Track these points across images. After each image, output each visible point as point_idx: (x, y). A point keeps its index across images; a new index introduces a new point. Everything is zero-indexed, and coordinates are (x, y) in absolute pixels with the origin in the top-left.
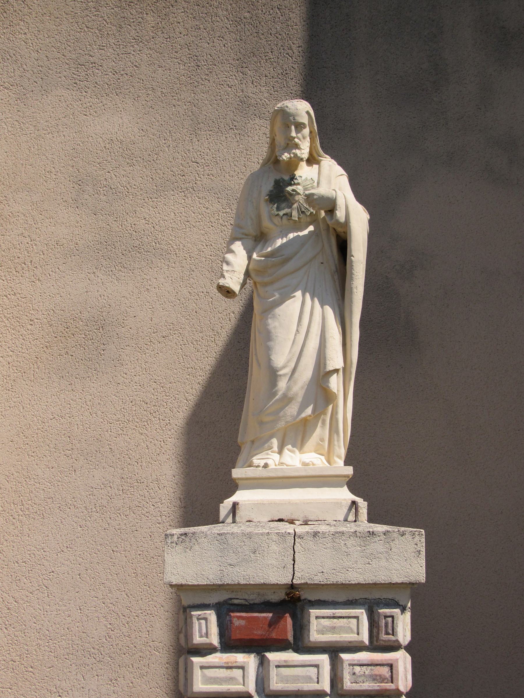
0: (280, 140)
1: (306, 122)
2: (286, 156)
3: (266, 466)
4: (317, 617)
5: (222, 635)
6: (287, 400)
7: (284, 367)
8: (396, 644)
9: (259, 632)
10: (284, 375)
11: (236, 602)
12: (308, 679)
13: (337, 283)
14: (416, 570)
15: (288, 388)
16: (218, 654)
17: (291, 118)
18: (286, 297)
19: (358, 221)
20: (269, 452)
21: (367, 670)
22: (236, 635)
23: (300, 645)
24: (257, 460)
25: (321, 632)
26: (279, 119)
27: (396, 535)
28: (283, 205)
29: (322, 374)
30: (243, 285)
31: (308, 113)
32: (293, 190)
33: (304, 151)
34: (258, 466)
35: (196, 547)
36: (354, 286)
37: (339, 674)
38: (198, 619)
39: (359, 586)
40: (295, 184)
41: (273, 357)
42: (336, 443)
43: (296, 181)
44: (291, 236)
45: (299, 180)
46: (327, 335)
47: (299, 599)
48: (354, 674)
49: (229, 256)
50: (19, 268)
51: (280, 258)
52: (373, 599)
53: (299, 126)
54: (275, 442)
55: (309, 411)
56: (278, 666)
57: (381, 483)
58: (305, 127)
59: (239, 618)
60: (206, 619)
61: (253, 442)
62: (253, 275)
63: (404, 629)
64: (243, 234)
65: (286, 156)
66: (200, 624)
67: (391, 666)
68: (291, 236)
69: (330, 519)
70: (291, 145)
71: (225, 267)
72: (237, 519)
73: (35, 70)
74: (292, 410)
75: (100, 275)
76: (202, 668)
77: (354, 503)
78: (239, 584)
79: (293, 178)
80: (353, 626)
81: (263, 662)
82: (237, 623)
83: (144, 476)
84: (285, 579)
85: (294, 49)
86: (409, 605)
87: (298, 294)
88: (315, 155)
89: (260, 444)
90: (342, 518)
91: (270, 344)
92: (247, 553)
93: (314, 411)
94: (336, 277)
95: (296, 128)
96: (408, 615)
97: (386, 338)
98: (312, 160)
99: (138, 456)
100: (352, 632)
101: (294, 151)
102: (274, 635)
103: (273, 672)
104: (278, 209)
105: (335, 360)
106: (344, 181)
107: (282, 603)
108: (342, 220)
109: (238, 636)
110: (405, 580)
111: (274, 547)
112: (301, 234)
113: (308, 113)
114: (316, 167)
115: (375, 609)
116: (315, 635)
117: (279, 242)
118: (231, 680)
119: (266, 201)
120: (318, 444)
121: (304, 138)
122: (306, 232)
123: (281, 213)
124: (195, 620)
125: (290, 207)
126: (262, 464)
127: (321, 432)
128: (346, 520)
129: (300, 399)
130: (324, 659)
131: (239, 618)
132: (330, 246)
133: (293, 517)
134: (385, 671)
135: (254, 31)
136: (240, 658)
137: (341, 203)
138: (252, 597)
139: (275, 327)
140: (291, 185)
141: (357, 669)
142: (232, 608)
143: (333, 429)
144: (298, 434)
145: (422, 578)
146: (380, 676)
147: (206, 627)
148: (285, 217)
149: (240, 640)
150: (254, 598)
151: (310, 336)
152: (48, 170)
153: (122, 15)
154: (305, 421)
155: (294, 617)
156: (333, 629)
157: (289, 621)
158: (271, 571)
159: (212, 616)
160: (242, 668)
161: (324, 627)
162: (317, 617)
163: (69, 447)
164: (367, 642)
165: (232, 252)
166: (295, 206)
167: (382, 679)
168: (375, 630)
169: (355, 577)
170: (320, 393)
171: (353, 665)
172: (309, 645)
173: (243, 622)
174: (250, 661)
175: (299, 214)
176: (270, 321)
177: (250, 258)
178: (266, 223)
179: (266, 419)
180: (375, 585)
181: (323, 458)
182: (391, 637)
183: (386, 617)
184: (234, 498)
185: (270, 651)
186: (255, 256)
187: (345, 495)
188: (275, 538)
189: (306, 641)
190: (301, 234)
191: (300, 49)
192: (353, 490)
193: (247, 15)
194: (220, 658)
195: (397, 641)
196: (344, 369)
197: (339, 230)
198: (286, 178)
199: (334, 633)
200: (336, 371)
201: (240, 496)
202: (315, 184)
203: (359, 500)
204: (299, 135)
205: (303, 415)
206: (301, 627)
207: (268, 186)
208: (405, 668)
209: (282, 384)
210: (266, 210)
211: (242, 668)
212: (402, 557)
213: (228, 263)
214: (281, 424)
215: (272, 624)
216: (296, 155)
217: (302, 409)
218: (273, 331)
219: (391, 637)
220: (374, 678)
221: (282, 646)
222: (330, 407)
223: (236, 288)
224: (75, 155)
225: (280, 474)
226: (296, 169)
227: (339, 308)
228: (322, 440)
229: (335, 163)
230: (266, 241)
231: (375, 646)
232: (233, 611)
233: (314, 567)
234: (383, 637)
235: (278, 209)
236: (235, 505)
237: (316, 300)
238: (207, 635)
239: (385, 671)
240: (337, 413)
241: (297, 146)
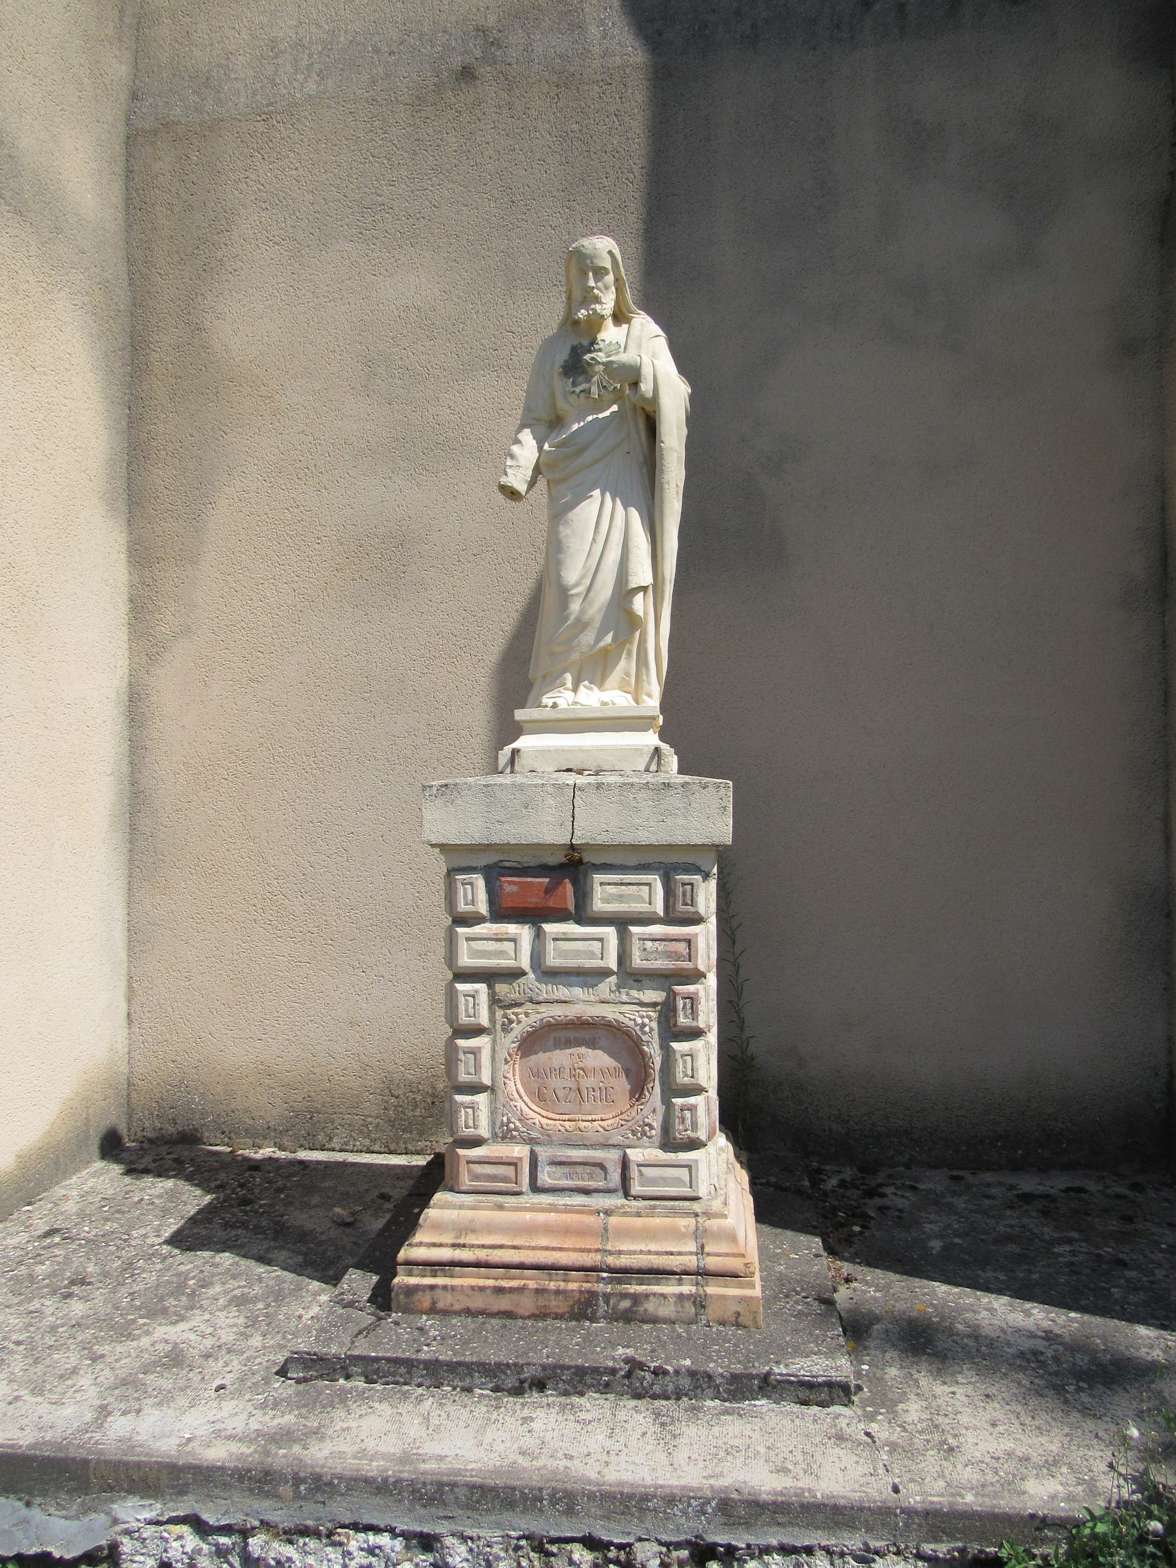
0: (577, 294)
1: (609, 266)
2: (582, 314)
3: (555, 706)
4: (602, 884)
5: (491, 902)
6: (581, 625)
7: (577, 585)
8: (696, 916)
9: (534, 900)
10: (578, 595)
11: (507, 864)
12: (592, 955)
13: (646, 479)
14: (722, 830)
15: (582, 611)
16: (487, 925)
17: (588, 261)
18: (581, 496)
19: (673, 395)
20: (561, 689)
21: (660, 946)
22: (508, 903)
23: (582, 916)
24: (547, 700)
25: (606, 900)
26: (574, 263)
27: (696, 788)
28: (581, 379)
29: (624, 592)
30: (532, 484)
31: (610, 253)
32: (593, 359)
33: (607, 304)
34: (546, 706)
35: (459, 801)
36: (665, 481)
37: (628, 949)
38: (463, 884)
39: (650, 847)
40: (595, 351)
41: (563, 574)
42: (645, 678)
43: (596, 347)
44: (590, 418)
45: (601, 345)
46: (631, 545)
47: (580, 862)
48: (645, 949)
49: (515, 449)
50: (301, 475)
51: (573, 449)
52: (670, 863)
53: (600, 273)
54: (568, 678)
55: (609, 638)
56: (555, 939)
57: (694, 727)
58: (607, 273)
59: (510, 883)
60: (471, 884)
61: (544, 677)
62: (543, 470)
63: (707, 899)
64: (534, 419)
65: (582, 314)
66: (465, 890)
67: (689, 942)
68: (590, 418)
69: (628, 769)
70: (588, 298)
71: (509, 462)
72: (516, 768)
73: (311, 218)
74: (588, 638)
75: (398, 481)
76: (468, 939)
77: (657, 750)
78: (508, 844)
79: (593, 342)
80: (649, 894)
81: (539, 935)
82: (508, 888)
83: (453, 722)
84: (564, 839)
85: (635, 171)
86: (715, 870)
87: (597, 493)
88: (625, 311)
89: (552, 681)
90: (642, 769)
91: (562, 556)
92: (518, 807)
93: (614, 639)
94: (644, 470)
95: (595, 274)
96: (713, 884)
97: (724, 548)
98: (620, 317)
99: (446, 699)
100: (644, 901)
101: (593, 306)
102: (551, 903)
103: (550, 946)
104: (574, 384)
105: (642, 574)
106: (661, 345)
107: (561, 866)
108: (650, 394)
109: (510, 904)
110: (707, 841)
111: (550, 801)
112: (601, 416)
113: (610, 253)
114: (625, 326)
115: (672, 873)
116: (599, 904)
117: (575, 427)
118: (501, 954)
119: (560, 374)
120: (623, 679)
121: (607, 288)
122: (607, 413)
123: (578, 390)
124: (459, 885)
125: (589, 381)
126: (550, 704)
127: (625, 665)
128: (647, 770)
129: (597, 625)
130: (610, 932)
131: (510, 883)
132: (638, 431)
133: (584, 767)
134: (682, 947)
135: (585, 149)
136: (512, 929)
137: (647, 372)
138: (526, 859)
139: (567, 536)
140: (590, 352)
141: (649, 944)
142: (503, 871)
143: (642, 662)
144: (596, 668)
145: (728, 839)
146: (676, 952)
147: (475, 894)
148: (582, 395)
149: (513, 908)
150: (529, 860)
151: (618, 546)
152: (331, 348)
153: (416, 136)
154: (605, 651)
155: (575, 883)
156: (620, 898)
157: (569, 887)
158: (547, 829)
159: (480, 881)
160: (514, 940)
161: (610, 895)
162: (602, 884)
163: (367, 688)
164: (662, 914)
165: (517, 442)
166: (595, 379)
167: (678, 957)
168: (671, 900)
169: (644, 837)
170: (622, 617)
171: (644, 940)
172: (592, 915)
173: (515, 888)
174: (524, 932)
175: (599, 391)
176: (561, 528)
177: (540, 448)
178: (561, 404)
179: (558, 649)
180: (671, 847)
181: (629, 696)
182: (691, 909)
183: (684, 884)
184: (515, 745)
185: (547, 921)
186: (546, 447)
187: (651, 739)
188: (550, 790)
189: (589, 910)
190: (601, 416)
191: (644, 171)
192: (662, 738)
193: (575, 127)
194: (489, 929)
195: (697, 912)
196: (655, 585)
197: (648, 408)
198: (585, 343)
199: (621, 902)
200: (644, 589)
201: (524, 742)
202: (622, 349)
203: (665, 747)
204: (600, 284)
205: (602, 644)
206: (583, 895)
207: (563, 355)
208: (708, 945)
209: (575, 606)
210: (561, 385)
211: (514, 940)
212: (707, 814)
213: (512, 457)
214: (575, 656)
215: (548, 891)
216: (595, 310)
217: (600, 636)
218: (564, 541)
219: (691, 909)
220: (669, 955)
221: (561, 916)
222: (637, 634)
223: (522, 488)
224: (364, 328)
225: (572, 716)
226: (599, 331)
227: (648, 509)
228: (628, 674)
229: (650, 319)
230: (563, 426)
231: (671, 917)
232: (503, 876)
233: (597, 825)
234: (680, 907)
235: (574, 384)
236: (515, 752)
237: (618, 500)
238: (473, 902)
239: (682, 947)
240: (645, 641)
241: (597, 300)
